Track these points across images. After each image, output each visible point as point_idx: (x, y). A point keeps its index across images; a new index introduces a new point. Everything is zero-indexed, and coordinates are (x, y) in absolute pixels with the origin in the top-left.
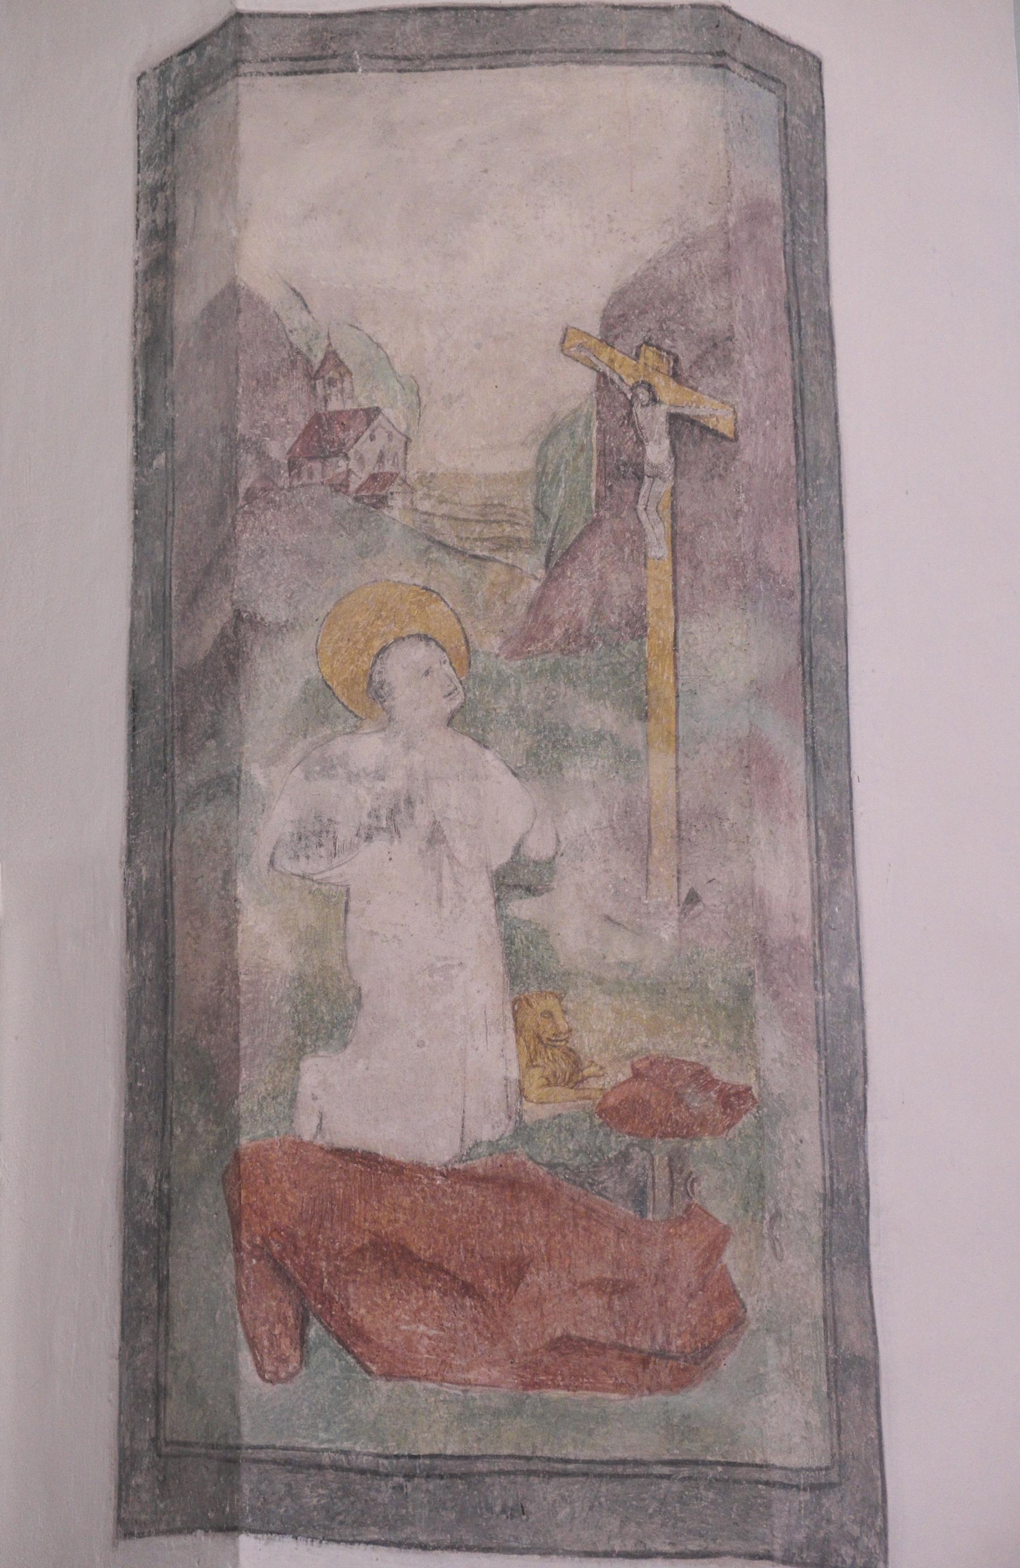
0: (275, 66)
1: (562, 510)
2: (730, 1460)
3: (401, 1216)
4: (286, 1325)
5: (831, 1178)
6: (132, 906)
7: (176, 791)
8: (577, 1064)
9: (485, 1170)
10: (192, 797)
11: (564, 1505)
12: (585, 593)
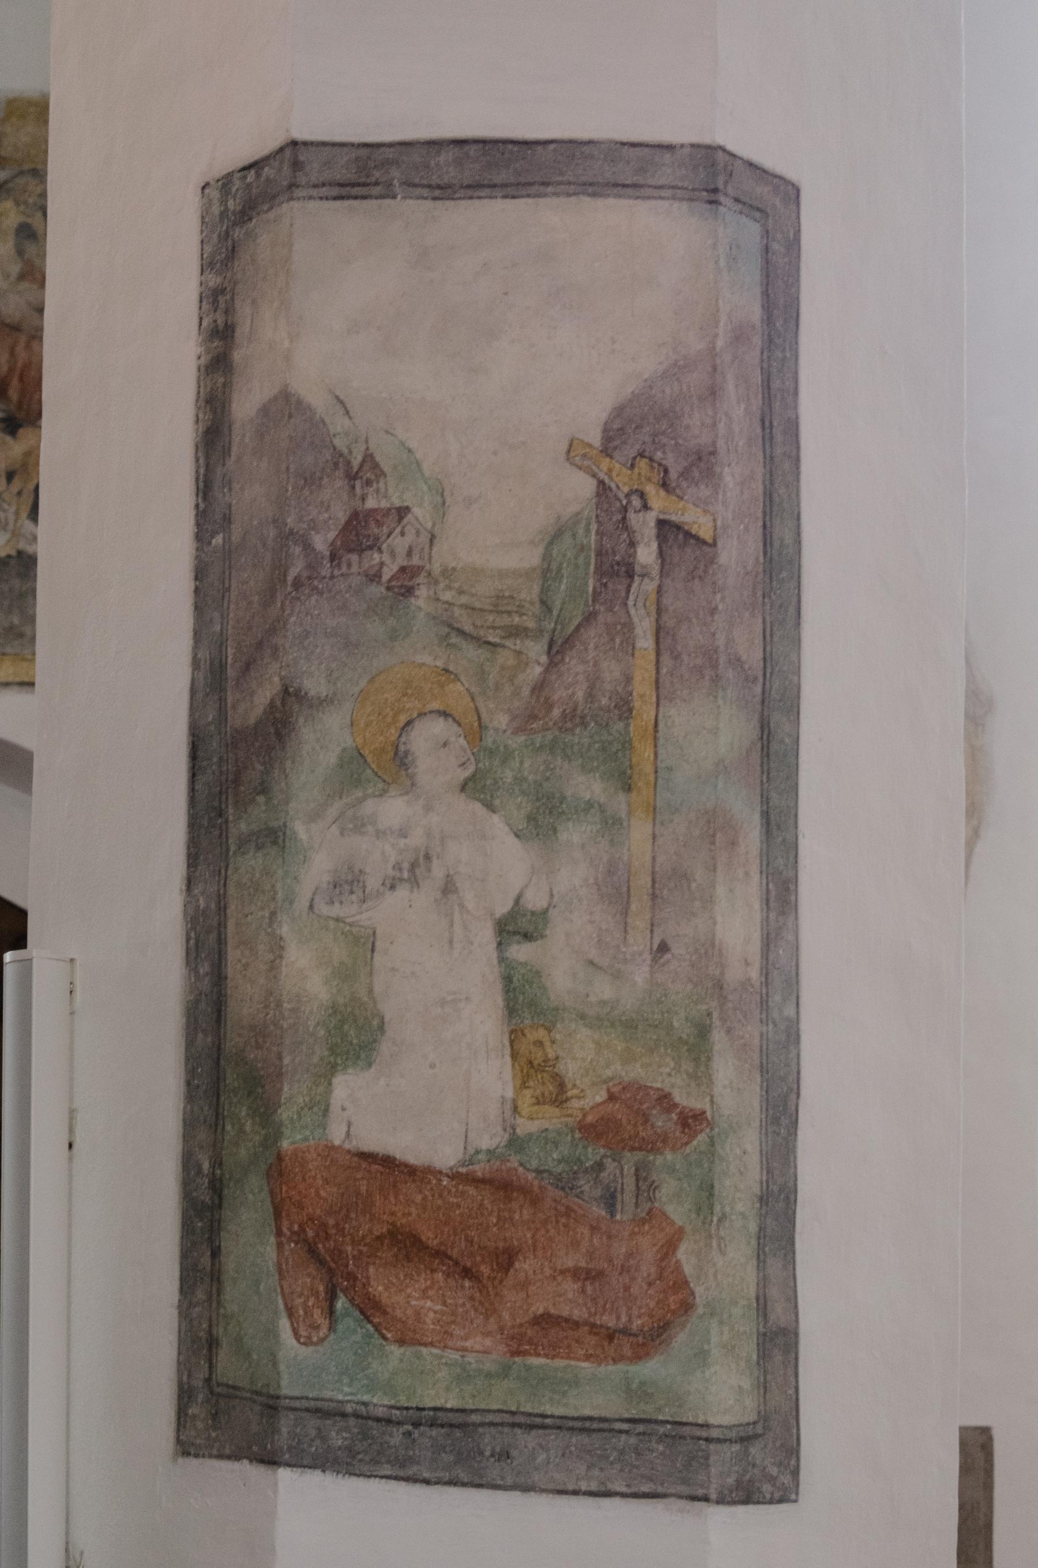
0: (324, 191)
1: (563, 603)
2: (678, 1419)
3: (413, 1210)
4: (317, 1298)
5: (767, 1182)
6: (192, 929)
7: (230, 835)
8: (561, 1086)
9: (483, 1174)
10: (243, 843)
11: (541, 1452)
12: (581, 678)
